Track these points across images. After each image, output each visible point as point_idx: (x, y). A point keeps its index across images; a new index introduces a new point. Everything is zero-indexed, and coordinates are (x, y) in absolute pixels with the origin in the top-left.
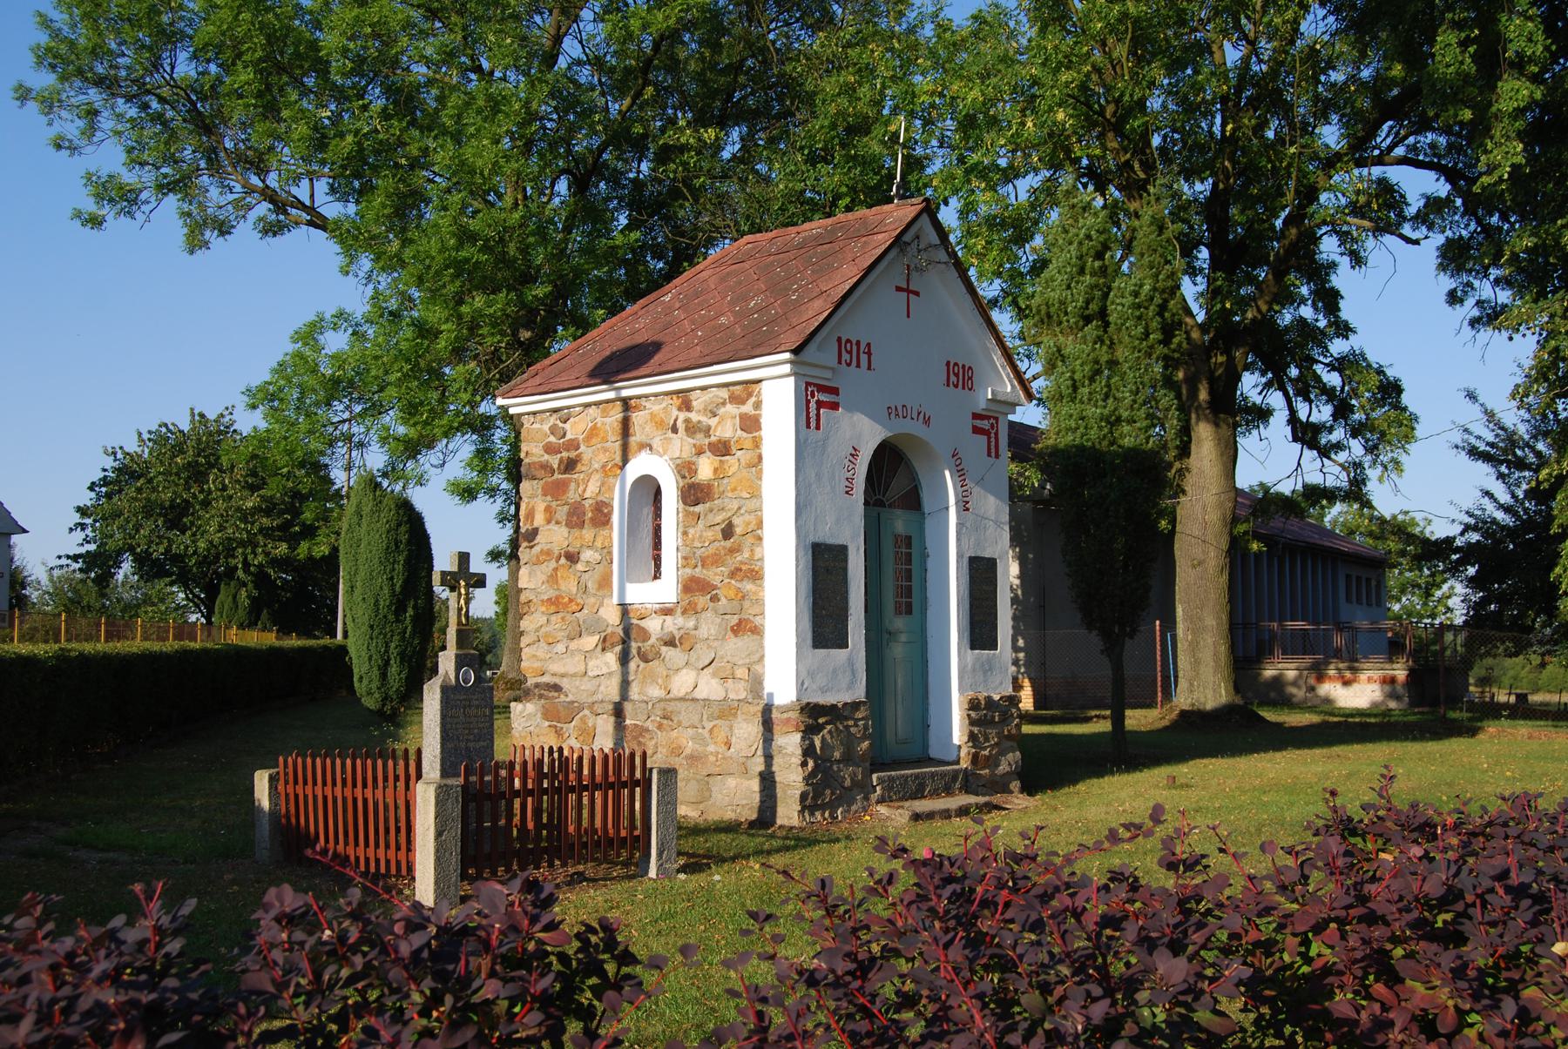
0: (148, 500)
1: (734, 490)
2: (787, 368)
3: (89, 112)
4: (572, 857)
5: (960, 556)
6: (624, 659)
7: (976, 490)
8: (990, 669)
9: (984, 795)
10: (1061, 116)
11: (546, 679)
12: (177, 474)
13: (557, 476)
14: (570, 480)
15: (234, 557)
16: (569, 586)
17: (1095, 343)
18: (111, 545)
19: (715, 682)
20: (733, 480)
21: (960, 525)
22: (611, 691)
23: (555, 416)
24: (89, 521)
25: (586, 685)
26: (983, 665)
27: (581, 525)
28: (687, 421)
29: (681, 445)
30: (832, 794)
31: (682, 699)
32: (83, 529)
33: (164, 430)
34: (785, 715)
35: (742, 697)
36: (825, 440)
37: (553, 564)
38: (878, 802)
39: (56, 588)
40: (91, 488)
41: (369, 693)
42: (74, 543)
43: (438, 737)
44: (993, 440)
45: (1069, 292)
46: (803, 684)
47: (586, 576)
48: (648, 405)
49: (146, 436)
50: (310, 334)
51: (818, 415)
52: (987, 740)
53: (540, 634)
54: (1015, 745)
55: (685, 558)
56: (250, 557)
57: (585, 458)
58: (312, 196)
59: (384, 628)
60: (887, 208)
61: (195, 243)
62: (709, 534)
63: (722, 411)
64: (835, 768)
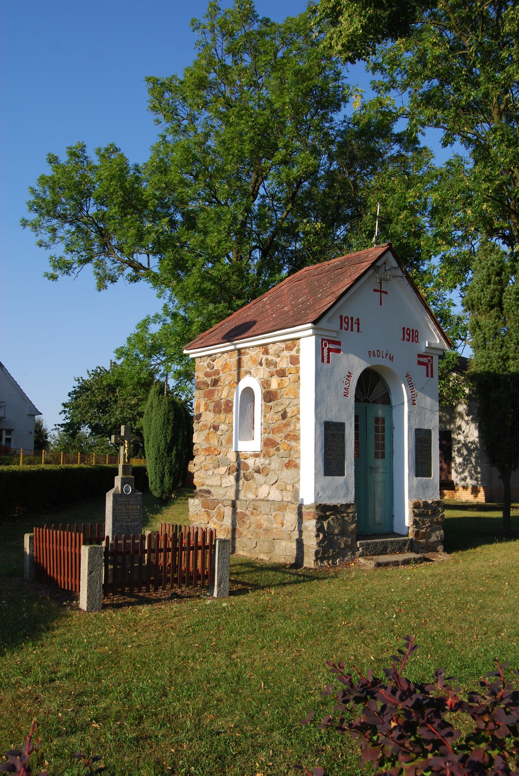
0: (91, 400)
1: (287, 394)
2: (311, 332)
3: (52, 230)
4: (184, 583)
5: (410, 428)
6: (237, 479)
7: (420, 394)
8: (427, 487)
9: (422, 553)
10: (484, 207)
11: (204, 488)
12: (104, 389)
13: (210, 388)
16: (214, 442)
17: (496, 319)
18: (75, 421)
19: (277, 492)
20: (287, 389)
21: (410, 412)
22: (231, 495)
23: (209, 358)
24: (67, 409)
25: (221, 491)
26: (422, 485)
27: (220, 412)
28: (267, 360)
29: (263, 372)
30: (334, 551)
31: (263, 500)
33: (99, 370)
34: (308, 510)
35: (289, 500)
36: (333, 368)
37: (207, 431)
38: (360, 556)
40: (69, 395)
41: (156, 490)
42: (61, 419)
44: (430, 368)
45: (482, 293)
46: (318, 494)
48: (249, 352)
50: (144, 325)
51: (329, 356)
52: (424, 524)
54: (441, 527)
55: (265, 429)
56: (133, 425)
57: (222, 379)
58: (149, 263)
60: (370, 249)
61: (101, 286)
62: (276, 417)
63: (282, 354)
64: (335, 538)
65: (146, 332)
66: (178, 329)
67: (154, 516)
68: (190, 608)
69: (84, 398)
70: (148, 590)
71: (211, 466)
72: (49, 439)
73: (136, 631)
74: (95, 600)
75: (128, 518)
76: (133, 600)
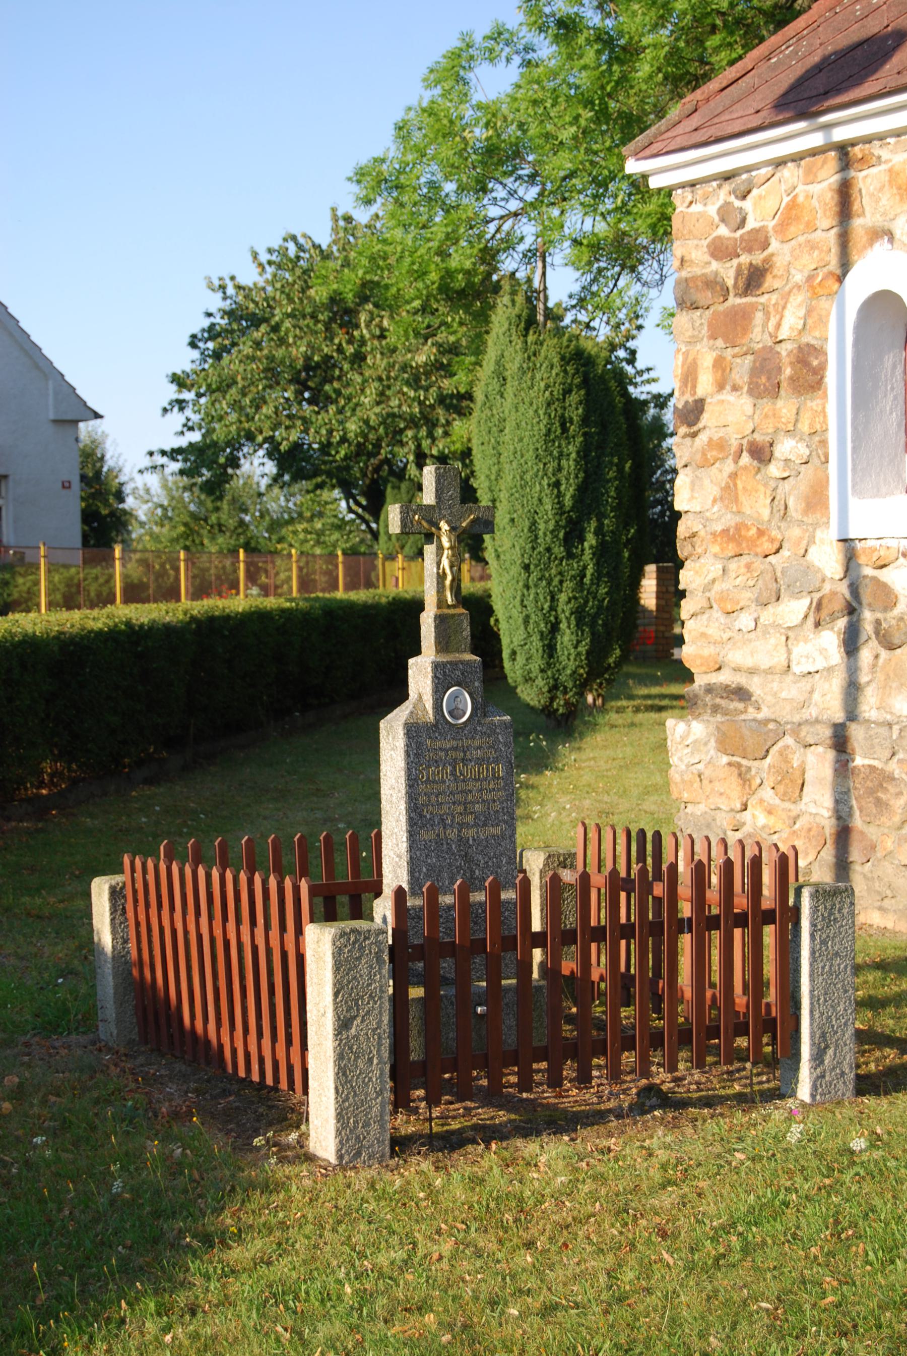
0: (271, 358)
11: (724, 678)
12: (313, 316)
14: (754, 307)
15: (402, 444)
18: (220, 433)
23: (727, 187)
24: (189, 396)
25: (791, 691)
27: (775, 391)
32: (182, 409)
37: (729, 466)
39: (173, 498)
40: (193, 345)
41: (528, 679)
43: (403, 819)
47: (787, 485)
48: (884, 154)
49: (264, 257)
53: (712, 594)
56: (425, 443)
57: (780, 263)
59: (547, 568)
65: (464, 97)
66: (584, 79)
67: (534, 779)
68: (718, 1148)
69: (247, 350)
70: (555, 1081)
71: (747, 596)
72: (130, 503)
73: (529, 1245)
74: (366, 1124)
75: (466, 812)
76: (502, 1117)
